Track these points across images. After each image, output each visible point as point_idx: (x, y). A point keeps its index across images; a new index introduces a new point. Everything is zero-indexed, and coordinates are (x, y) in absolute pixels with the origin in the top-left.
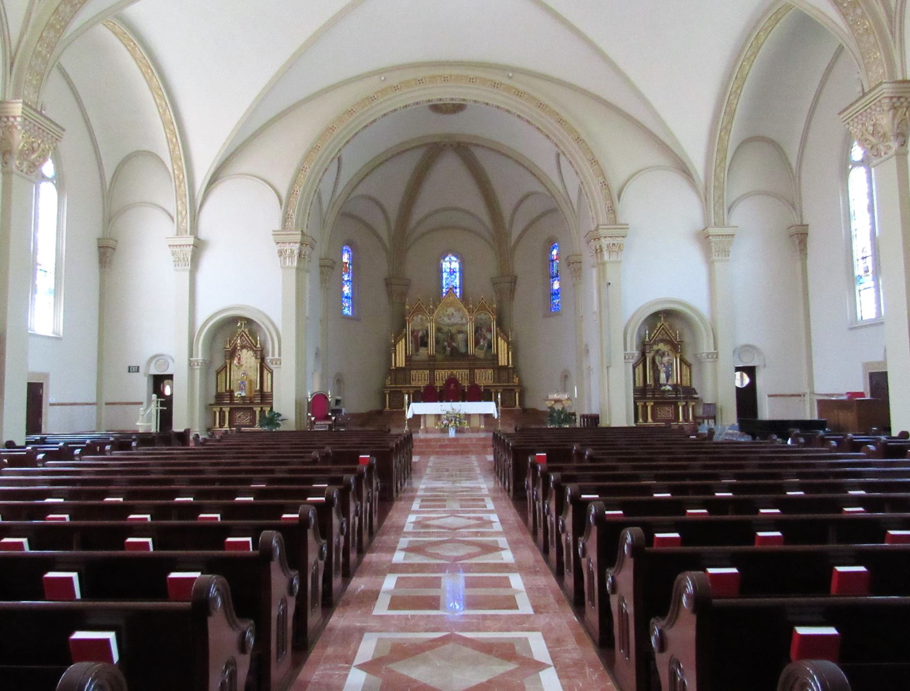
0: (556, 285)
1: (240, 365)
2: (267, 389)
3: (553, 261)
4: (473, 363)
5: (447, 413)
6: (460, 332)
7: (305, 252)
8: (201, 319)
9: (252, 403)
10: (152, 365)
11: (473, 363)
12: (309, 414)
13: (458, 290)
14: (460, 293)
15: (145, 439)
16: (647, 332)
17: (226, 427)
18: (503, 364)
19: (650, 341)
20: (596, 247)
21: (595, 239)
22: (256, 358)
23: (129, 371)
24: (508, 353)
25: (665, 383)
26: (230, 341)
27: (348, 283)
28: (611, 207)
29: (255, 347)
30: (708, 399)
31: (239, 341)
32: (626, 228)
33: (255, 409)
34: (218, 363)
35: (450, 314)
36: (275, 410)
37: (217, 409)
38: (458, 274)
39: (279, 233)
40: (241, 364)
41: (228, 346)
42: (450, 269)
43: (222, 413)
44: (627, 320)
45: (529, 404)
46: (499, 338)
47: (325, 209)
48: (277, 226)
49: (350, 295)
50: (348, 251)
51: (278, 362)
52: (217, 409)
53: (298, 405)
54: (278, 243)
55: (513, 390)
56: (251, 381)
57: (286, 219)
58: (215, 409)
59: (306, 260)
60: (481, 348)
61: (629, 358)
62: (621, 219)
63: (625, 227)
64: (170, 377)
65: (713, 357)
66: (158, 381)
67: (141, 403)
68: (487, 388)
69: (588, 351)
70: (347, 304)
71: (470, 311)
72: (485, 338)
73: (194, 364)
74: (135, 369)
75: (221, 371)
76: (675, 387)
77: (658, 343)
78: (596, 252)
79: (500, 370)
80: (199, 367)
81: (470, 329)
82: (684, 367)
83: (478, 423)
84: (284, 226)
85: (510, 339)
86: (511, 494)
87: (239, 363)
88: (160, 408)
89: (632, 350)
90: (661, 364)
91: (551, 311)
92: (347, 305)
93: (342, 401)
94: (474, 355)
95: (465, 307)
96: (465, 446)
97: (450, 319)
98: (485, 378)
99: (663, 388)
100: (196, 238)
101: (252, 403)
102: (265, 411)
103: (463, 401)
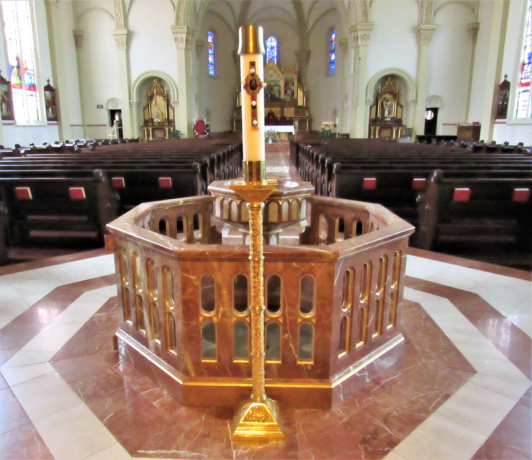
0: (333, 57)
1: (156, 104)
2: (171, 118)
3: (332, 41)
4: (283, 104)
5: (268, 131)
6: (276, 85)
7: (189, 38)
8: (133, 79)
9: (163, 125)
10: (110, 105)
11: (283, 104)
12: (195, 132)
13: (275, 59)
14: (277, 61)
15: (115, 142)
16: (380, 87)
17: (151, 138)
18: (300, 105)
19: (381, 92)
20: (354, 36)
21: (354, 31)
22: (165, 100)
23: (98, 108)
24: (303, 99)
25: (387, 116)
26: (150, 91)
27: (212, 55)
28: (365, 11)
29: (164, 94)
30: (409, 127)
31: (155, 91)
32: (372, 25)
33: (165, 129)
34: (144, 103)
35: (271, 74)
36: (176, 129)
37: (145, 129)
38: (276, 49)
39: (174, 27)
40: (157, 103)
41: (149, 94)
42: (271, 46)
43: (148, 131)
44: (369, 80)
45: (315, 128)
46: (299, 90)
47: (198, 9)
48: (173, 22)
49: (213, 63)
50: (211, 35)
51: (177, 103)
52: (145, 129)
53: (189, 126)
54: (174, 33)
55: (305, 120)
56: (162, 113)
57: (178, 18)
58: (144, 129)
59: (190, 43)
60: (288, 95)
61: (368, 102)
62: (371, 18)
63: (372, 24)
64: (119, 111)
65: (414, 102)
66: (113, 113)
67: (106, 125)
68: (291, 119)
69: (347, 98)
70: (211, 68)
71: (283, 73)
72: (290, 89)
73: (132, 104)
74: (100, 107)
75: (146, 107)
76: (392, 118)
77: (386, 93)
78: (354, 40)
79: (299, 109)
80: (134, 105)
81: (282, 83)
82: (399, 107)
83: (284, 137)
84: (177, 24)
85: (305, 90)
86: (295, 164)
87: (156, 103)
88: (118, 128)
89: (370, 98)
90: (386, 106)
91: (329, 73)
92: (211, 69)
93: (210, 126)
94: (284, 100)
95: (279, 70)
96: (276, 148)
97: (270, 77)
98: (289, 112)
99: (386, 119)
100: (128, 30)
101: (163, 125)
102: (171, 130)
103: (277, 125)
